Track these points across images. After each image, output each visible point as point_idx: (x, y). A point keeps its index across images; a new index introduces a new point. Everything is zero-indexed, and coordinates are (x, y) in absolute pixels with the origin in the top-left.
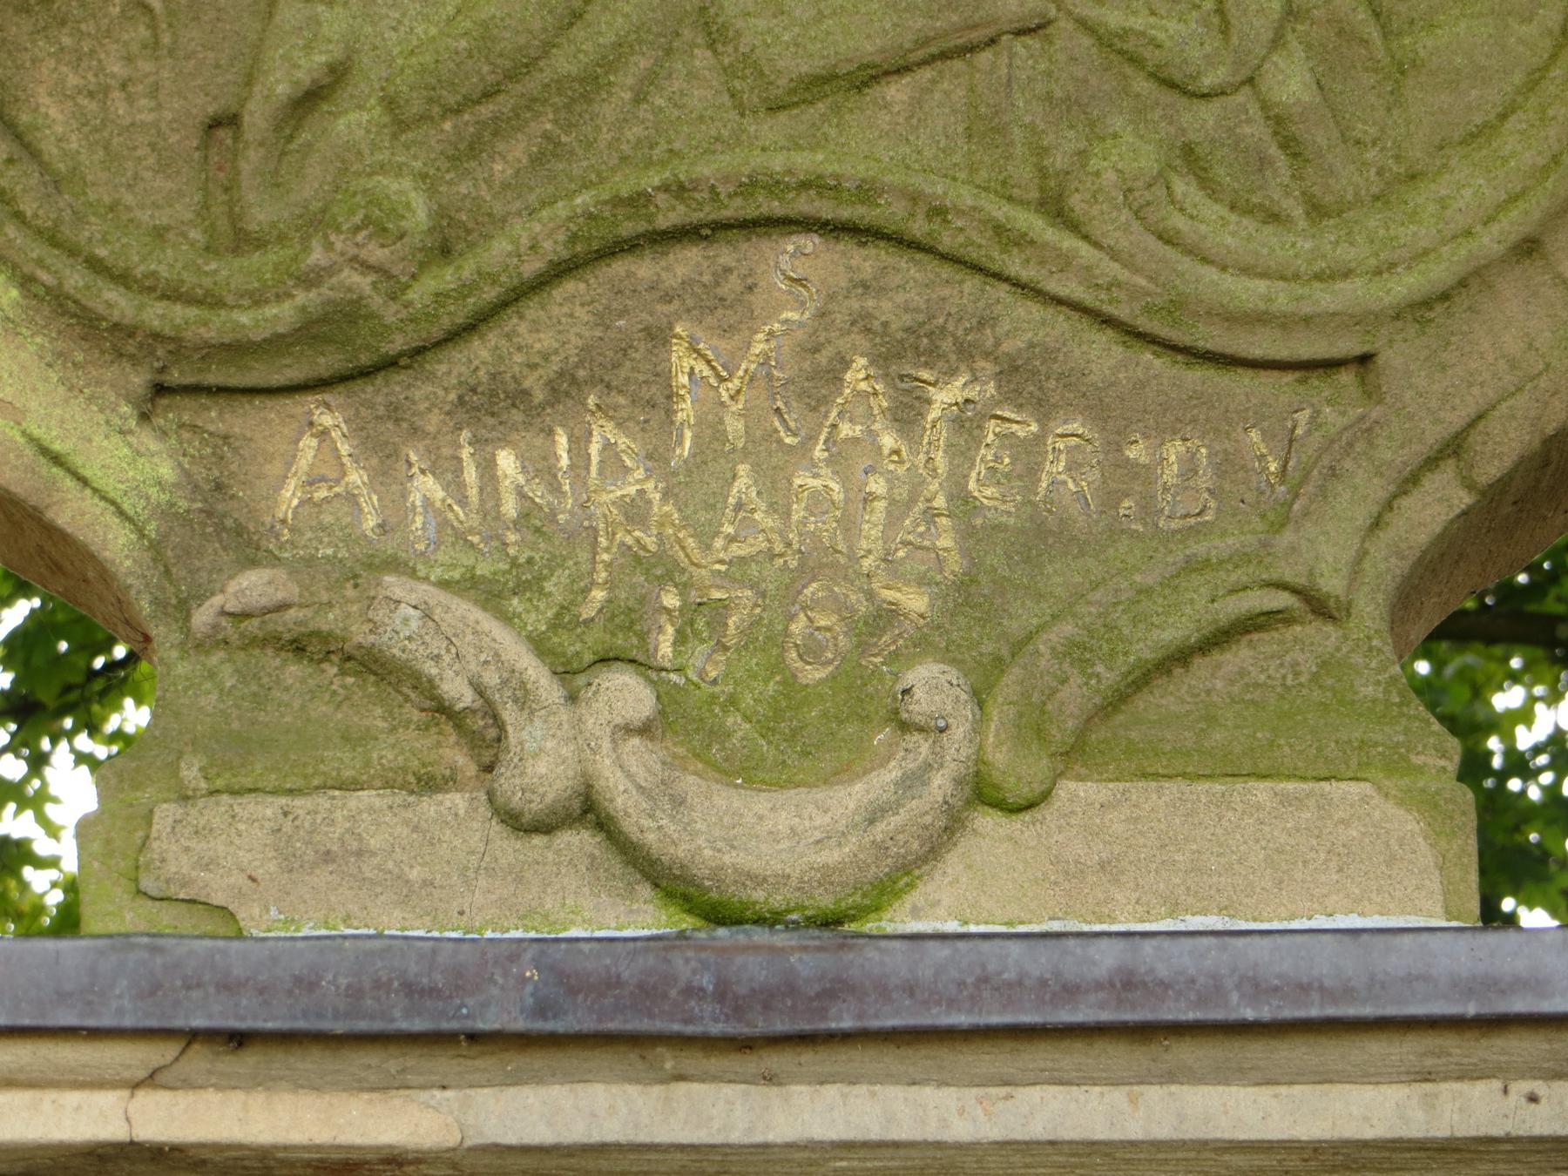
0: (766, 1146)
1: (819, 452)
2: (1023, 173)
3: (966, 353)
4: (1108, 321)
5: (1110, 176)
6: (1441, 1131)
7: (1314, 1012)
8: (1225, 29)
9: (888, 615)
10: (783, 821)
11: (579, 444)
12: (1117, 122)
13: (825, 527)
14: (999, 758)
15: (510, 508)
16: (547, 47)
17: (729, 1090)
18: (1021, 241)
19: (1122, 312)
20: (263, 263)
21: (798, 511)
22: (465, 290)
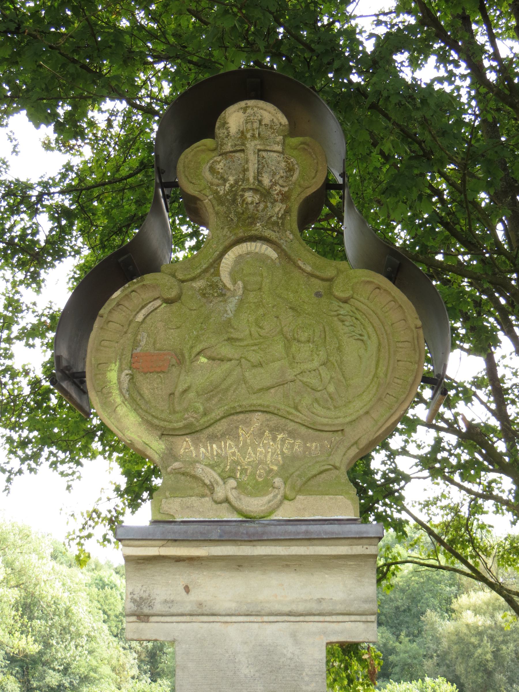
0: (253, 556)
1: (261, 445)
2: (291, 403)
3: (283, 430)
4: (304, 425)
5: (304, 404)
6: (353, 553)
7: (334, 537)
8: (321, 381)
9: (271, 470)
10: (256, 502)
11: (225, 444)
12: (305, 395)
13: (262, 457)
14: (288, 493)
15: (215, 453)
16: (220, 384)
17: (248, 547)
18: (291, 414)
19: (306, 424)
20: (178, 416)
21: (258, 454)
22: (208, 421)
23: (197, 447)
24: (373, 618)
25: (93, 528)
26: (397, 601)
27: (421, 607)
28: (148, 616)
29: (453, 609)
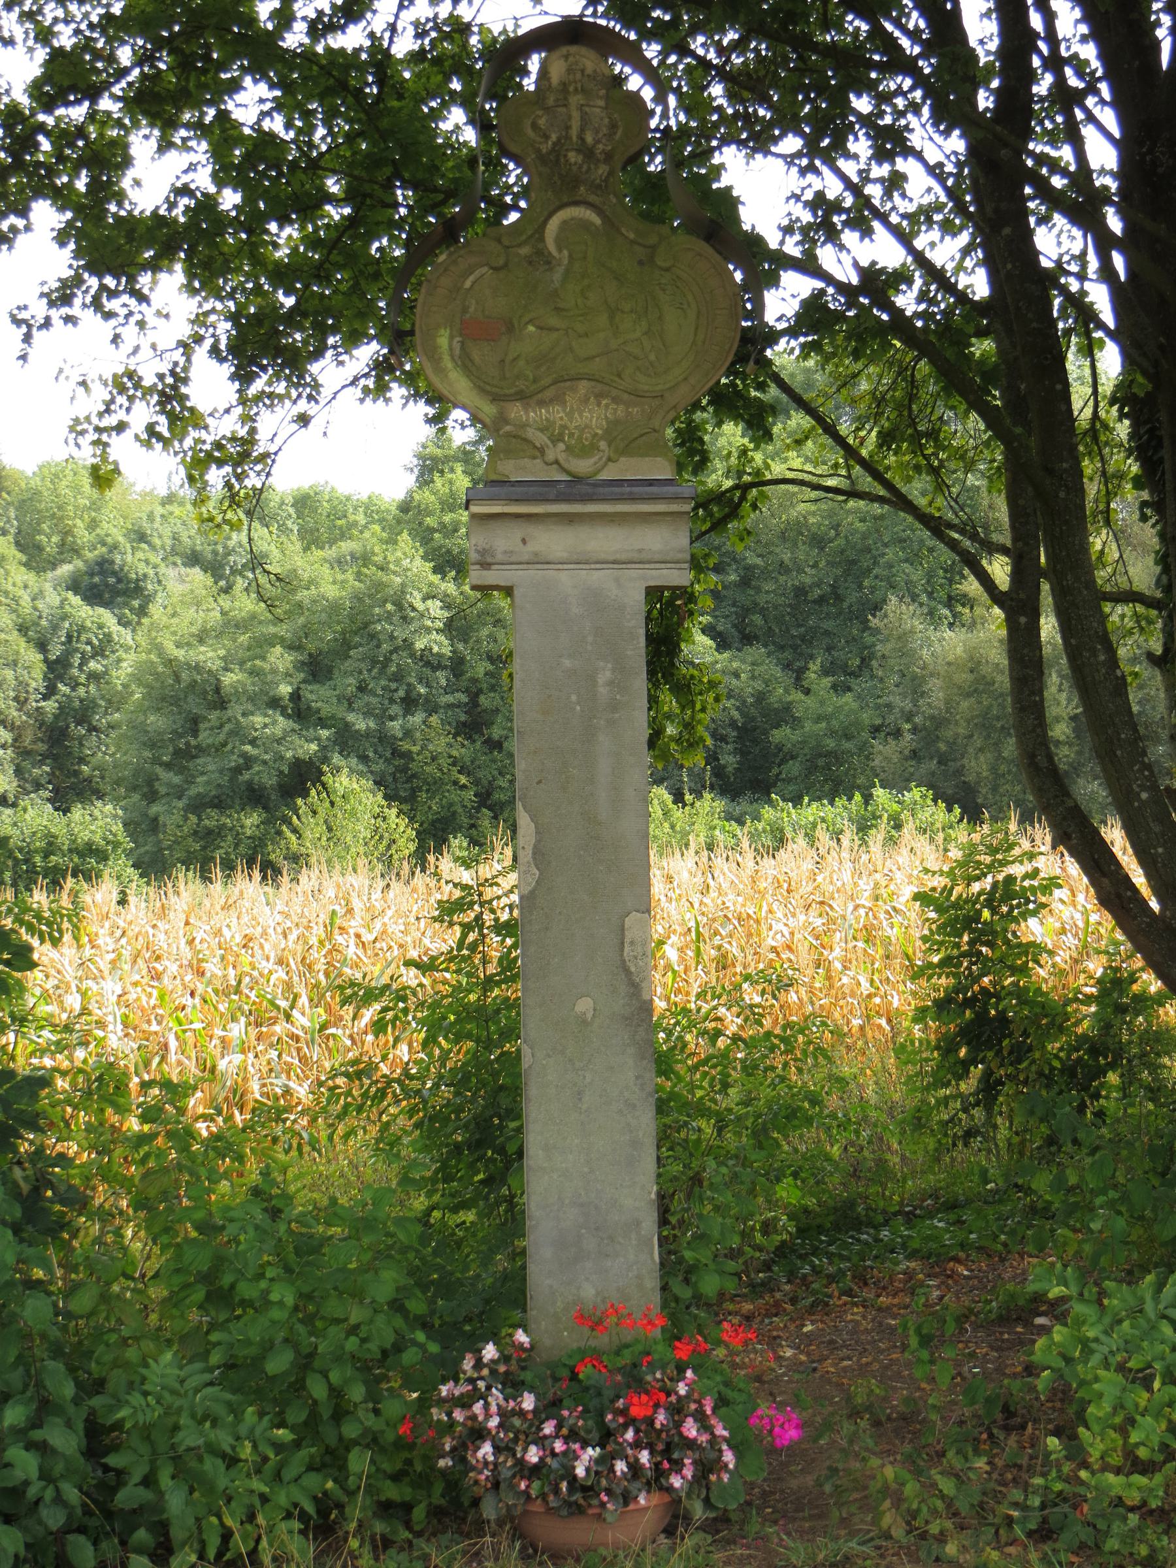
23: (527, 413)
24: (686, 565)
25: (128, 410)
26: (800, 570)
27: (873, 589)
28: (490, 564)
29: (965, 596)
